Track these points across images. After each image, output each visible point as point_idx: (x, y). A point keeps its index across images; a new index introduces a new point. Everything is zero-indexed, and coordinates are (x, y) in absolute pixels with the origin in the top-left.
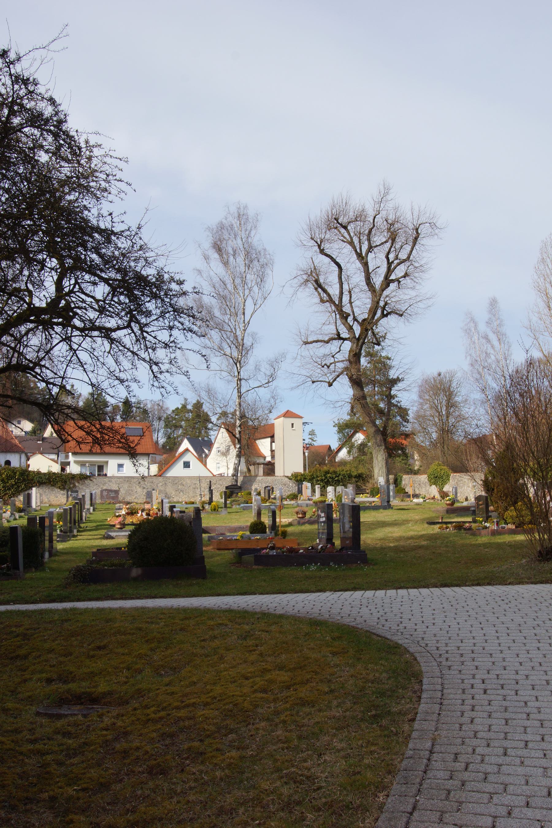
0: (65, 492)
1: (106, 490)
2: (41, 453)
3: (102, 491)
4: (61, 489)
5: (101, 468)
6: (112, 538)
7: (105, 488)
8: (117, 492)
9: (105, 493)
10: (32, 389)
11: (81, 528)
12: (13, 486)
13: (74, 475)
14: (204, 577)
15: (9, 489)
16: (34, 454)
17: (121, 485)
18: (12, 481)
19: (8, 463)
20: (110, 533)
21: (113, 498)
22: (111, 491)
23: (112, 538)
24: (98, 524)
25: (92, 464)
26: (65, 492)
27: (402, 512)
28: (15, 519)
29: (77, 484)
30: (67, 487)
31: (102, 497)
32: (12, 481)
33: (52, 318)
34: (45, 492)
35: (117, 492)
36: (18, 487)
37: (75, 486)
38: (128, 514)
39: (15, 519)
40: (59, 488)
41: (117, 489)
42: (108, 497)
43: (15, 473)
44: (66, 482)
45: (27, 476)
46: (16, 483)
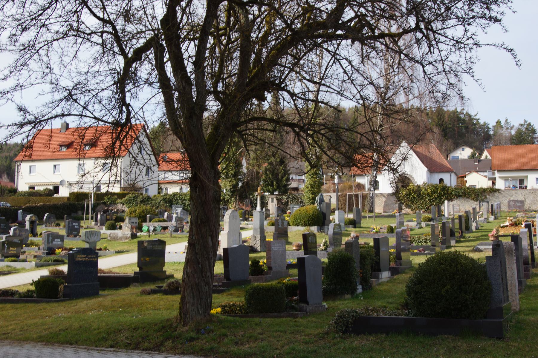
0: (478, 203)
1: (513, 200)
2: (477, 172)
3: (509, 202)
4: (475, 201)
5: (521, 181)
6: (480, 251)
7: (512, 199)
8: (522, 202)
9: (512, 203)
10: (475, 124)
11: (464, 237)
12: (436, 198)
13: (485, 189)
14: (498, 333)
15: (433, 201)
16: (471, 172)
17: (526, 197)
18: (436, 195)
19: (441, 180)
20: (479, 247)
21: (519, 207)
22: (518, 201)
23: (480, 251)
24: (483, 233)
25: (514, 179)
26: (478, 203)
27: (506, 237)
28: (421, 228)
29: (488, 196)
30: (479, 199)
31: (509, 206)
32: (436, 195)
33: (336, 31)
34: (462, 203)
35: (522, 202)
36: (441, 199)
37: (486, 198)
38: (512, 225)
39: (421, 228)
40: (473, 199)
41: (523, 199)
42: (515, 206)
43: (438, 189)
44: (478, 195)
45: (447, 191)
46: (438, 197)
